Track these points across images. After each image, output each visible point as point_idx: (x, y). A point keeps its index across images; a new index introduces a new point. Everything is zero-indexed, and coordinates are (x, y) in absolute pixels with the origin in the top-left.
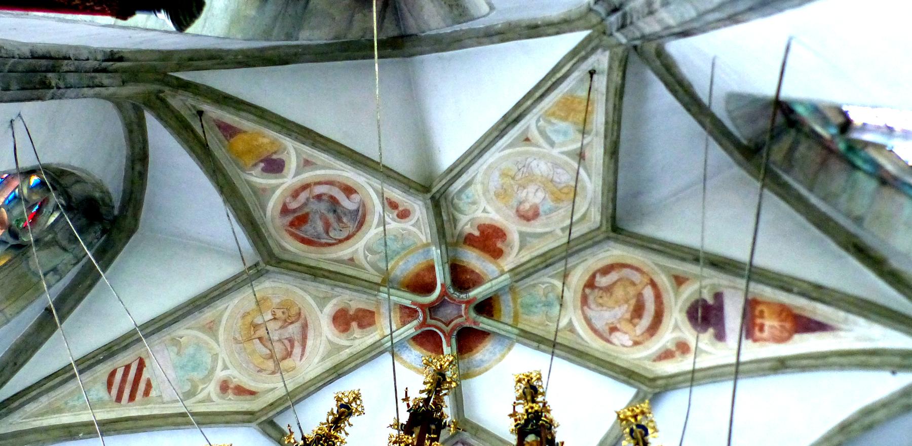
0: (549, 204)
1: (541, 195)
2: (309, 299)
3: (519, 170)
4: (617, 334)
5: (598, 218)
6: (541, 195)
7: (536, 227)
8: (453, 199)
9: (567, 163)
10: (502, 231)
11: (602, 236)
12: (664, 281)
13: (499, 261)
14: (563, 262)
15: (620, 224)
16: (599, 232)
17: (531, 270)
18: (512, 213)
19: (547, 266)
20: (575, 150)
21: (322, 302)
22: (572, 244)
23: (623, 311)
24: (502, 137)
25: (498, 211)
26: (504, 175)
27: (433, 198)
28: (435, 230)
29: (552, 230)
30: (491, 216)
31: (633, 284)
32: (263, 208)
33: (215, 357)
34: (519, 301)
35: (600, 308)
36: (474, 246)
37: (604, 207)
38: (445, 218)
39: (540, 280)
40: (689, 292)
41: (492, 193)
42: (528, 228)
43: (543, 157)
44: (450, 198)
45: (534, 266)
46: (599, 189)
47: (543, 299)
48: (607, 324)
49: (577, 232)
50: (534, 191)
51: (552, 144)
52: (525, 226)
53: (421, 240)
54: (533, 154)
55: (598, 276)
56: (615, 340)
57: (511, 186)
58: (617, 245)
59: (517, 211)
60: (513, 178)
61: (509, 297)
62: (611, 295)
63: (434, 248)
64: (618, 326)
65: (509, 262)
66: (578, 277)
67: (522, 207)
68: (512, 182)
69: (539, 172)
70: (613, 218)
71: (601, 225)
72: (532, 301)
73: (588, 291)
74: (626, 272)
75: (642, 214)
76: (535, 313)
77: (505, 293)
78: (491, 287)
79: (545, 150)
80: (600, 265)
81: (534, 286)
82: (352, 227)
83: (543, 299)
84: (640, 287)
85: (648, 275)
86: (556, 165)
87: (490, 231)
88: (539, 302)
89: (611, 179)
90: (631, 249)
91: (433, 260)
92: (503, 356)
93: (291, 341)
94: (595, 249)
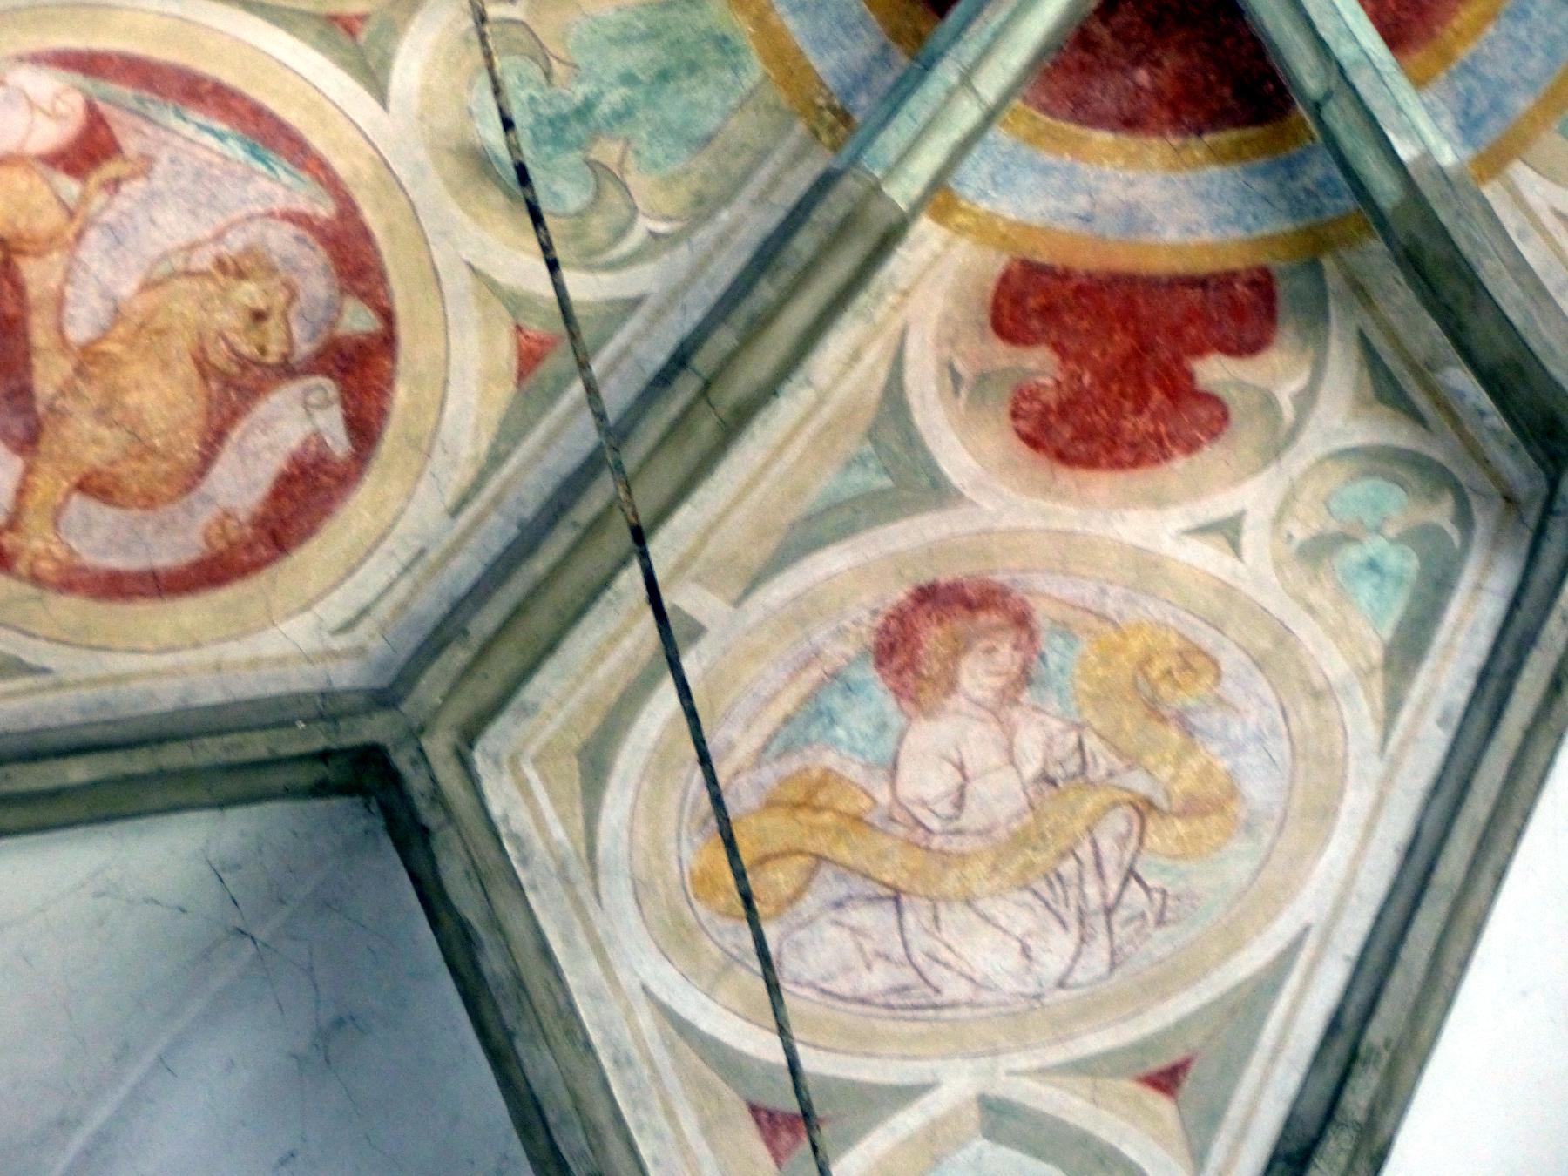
0: (842, 753)
1: (924, 781)
3: (1131, 874)
4: (51, 134)
5: (500, 797)
6: (924, 781)
7: (856, 577)
8: (1464, 519)
9: (863, 1043)
10: (1063, 457)
11: (430, 688)
13: (996, 263)
14: (617, 396)
15: (342, 816)
16: (461, 709)
17: (766, 291)
18: (1048, 595)
19: (680, 360)
20: (848, 1140)
22: (617, 538)
24: (1334, 1026)
25: (1146, 568)
26: (1212, 804)
28: (1493, 273)
29: (765, 576)
30: (1177, 518)
34: (755, 69)
35: (235, 242)
36: (1199, 282)
37: (497, 871)
38: (1460, 379)
39: (682, 256)
41: (1231, 659)
42: (909, 545)
43: (1026, 1015)
44: (1484, 520)
45: (761, 324)
46: (580, 974)
47: (608, 151)
48: (146, 166)
49: (615, 635)
50: (976, 788)
51: (999, 1118)
52: (932, 552)
53: (1550, 174)
54: (1090, 1009)
55: (339, 443)
56: (45, 84)
57: (1133, 761)
58: (302, 679)
59: (1022, 620)
60: (1144, 808)
61: (824, 65)
62: (203, 365)
63: (1447, 156)
64: (70, 187)
65: (931, 283)
66: (456, 382)
67: (1006, 655)
68: (1139, 783)
69: (1000, 910)
70: (410, 835)
71: (465, 763)
72: (672, 107)
73: (358, 320)
74: (174, 543)
75: (242, 938)
76: (624, 39)
77: (862, 80)
78: (967, 79)
79: (1022, 1061)
80: (357, 514)
81: (702, 208)
83: (608, 151)
84: (48, 484)
85: (36, 579)
86: (916, 1001)
87: (1136, 424)
88: (623, 114)
89: (538, 1064)
90: (211, 694)
91: (1419, 83)
94: (430, 605)
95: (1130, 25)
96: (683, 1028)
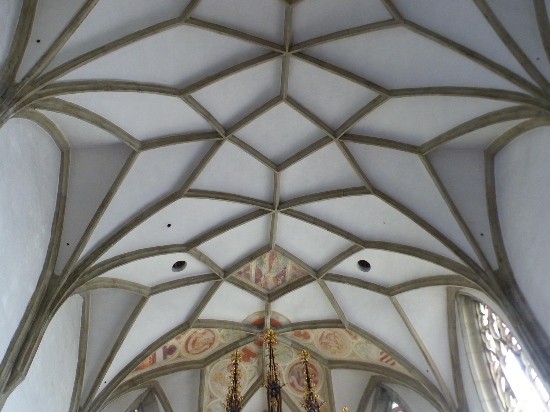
2: (317, 346)
12: (185, 354)
21: (312, 344)
23: (199, 340)
27: (286, 99)
31: (195, 350)
32: (323, 387)
33: (355, 347)
40: (176, 354)
82: (295, 369)
92: (247, 317)
93: (327, 337)
95: (154, 361)
96: (210, 390)
